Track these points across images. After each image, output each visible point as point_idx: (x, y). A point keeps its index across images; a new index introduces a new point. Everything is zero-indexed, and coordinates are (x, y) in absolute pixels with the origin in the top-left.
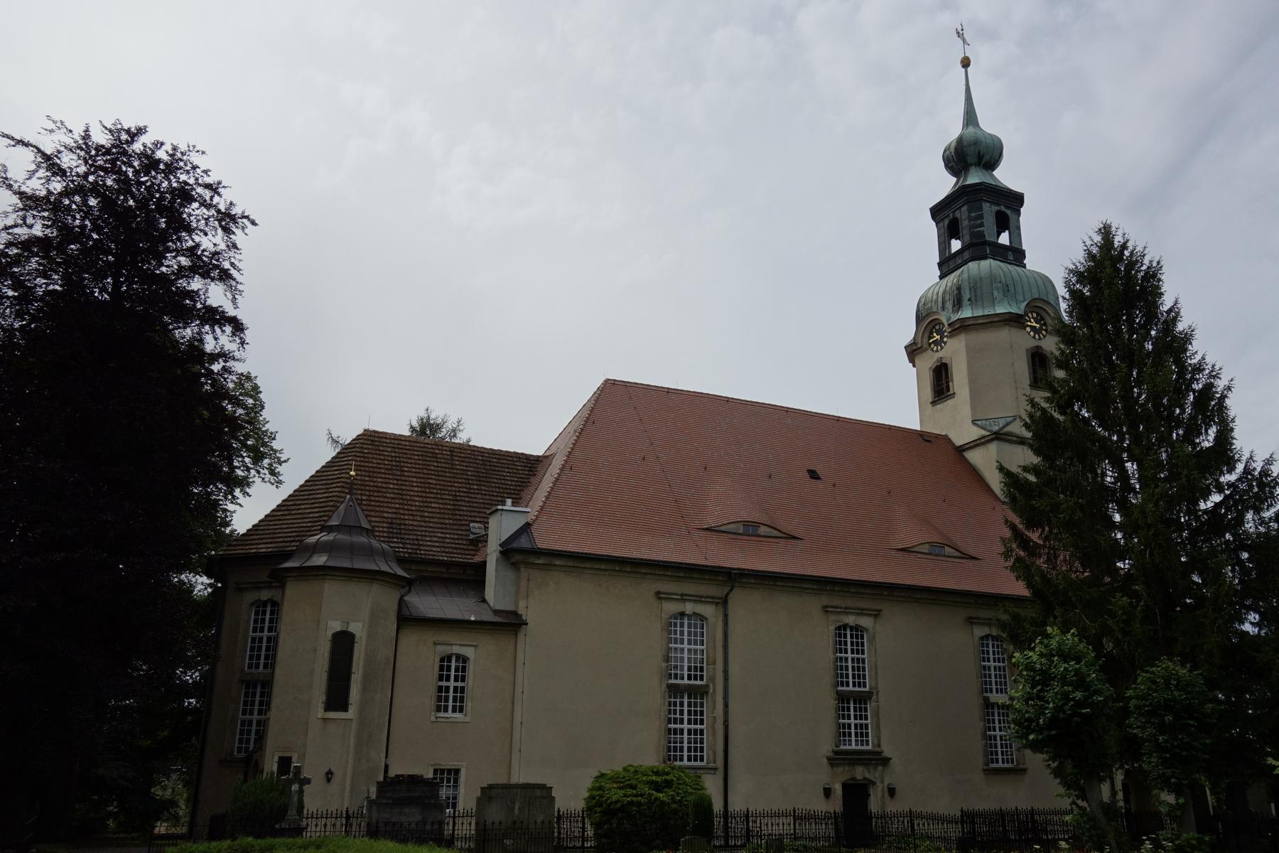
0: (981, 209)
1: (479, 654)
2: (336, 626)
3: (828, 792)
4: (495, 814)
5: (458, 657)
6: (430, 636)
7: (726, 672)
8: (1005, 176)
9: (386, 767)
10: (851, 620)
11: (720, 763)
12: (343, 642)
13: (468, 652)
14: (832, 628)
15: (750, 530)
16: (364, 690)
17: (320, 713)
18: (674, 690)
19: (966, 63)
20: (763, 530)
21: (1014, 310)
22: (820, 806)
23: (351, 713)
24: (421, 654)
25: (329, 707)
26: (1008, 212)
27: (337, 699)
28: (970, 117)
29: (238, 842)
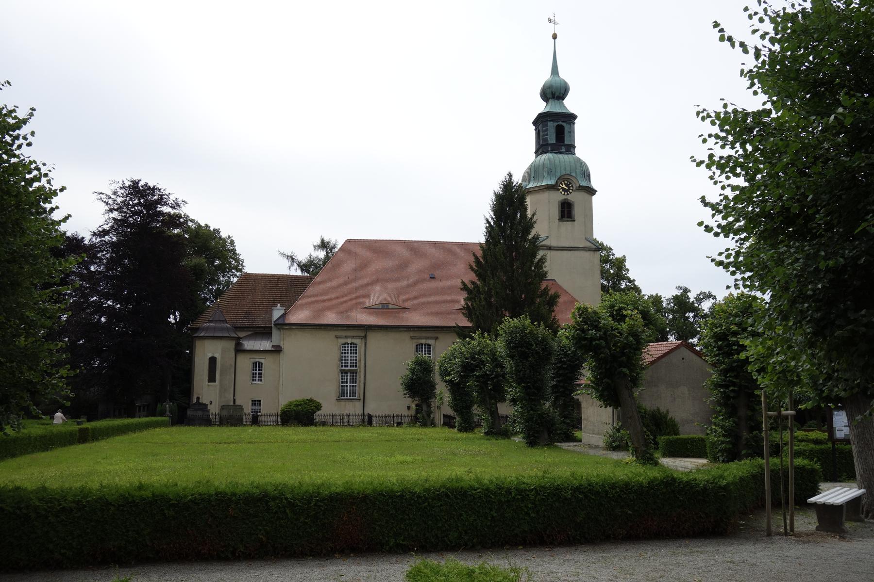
0: (547, 125)
1: (267, 362)
2: (210, 355)
3: (409, 408)
4: (225, 413)
5: (259, 363)
6: (248, 356)
7: (365, 364)
8: (570, 104)
9: (234, 400)
10: (423, 341)
11: (362, 397)
12: (213, 360)
13: (262, 361)
14: (414, 345)
15: (385, 307)
16: (221, 375)
17: (207, 383)
18: (343, 372)
19: (555, 37)
20: (391, 306)
21: (549, 183)
22: (405, 412)
23: (217, 383)
24: (245, 363)
25: (209, 381)
26: (564, 124)
27: (212, 378)
28: (555, 70)
29: (456, 424)
